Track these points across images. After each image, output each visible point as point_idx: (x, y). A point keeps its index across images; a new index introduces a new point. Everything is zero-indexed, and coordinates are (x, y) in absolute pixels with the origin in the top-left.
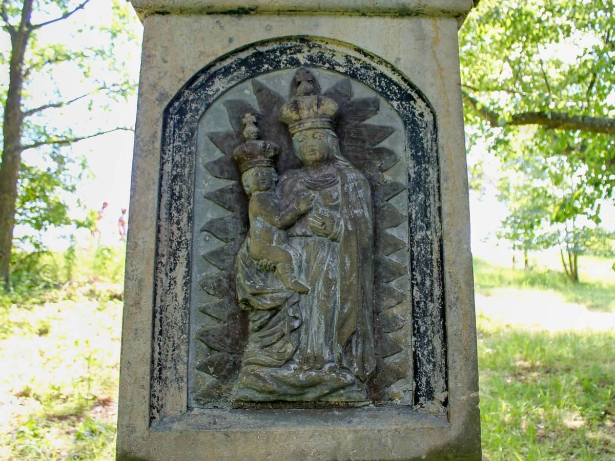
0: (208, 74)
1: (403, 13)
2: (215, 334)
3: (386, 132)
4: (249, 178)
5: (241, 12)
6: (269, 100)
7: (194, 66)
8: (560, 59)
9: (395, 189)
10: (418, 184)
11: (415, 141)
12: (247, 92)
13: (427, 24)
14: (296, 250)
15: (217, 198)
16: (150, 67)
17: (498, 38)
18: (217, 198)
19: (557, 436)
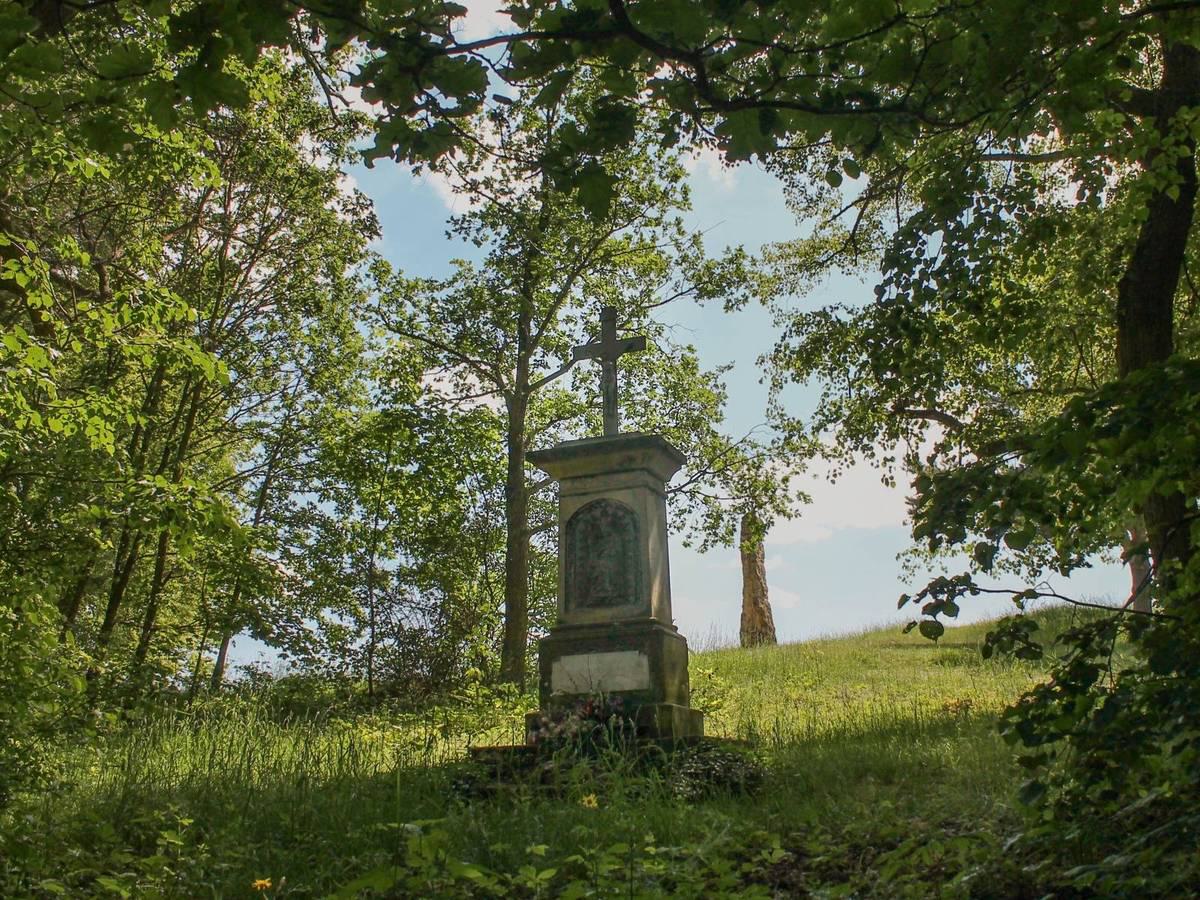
0: (577, 514)
1: (628, 488)
2: (762, 511)
3: (627, 524)
4: (590, 541)
5: (584, 494)
6: (594, 519)
7: (573, 511)
8: (801, 386)
9: (629, 541)
10: (636, 538)
11: (635, 527)
12: (589, 517)
13: (637, 490)
14: (602, 562)
15: (582, 549)
16: (467, 396)
17: (807, 274)
18: (582, 549)
19: (876, 802)
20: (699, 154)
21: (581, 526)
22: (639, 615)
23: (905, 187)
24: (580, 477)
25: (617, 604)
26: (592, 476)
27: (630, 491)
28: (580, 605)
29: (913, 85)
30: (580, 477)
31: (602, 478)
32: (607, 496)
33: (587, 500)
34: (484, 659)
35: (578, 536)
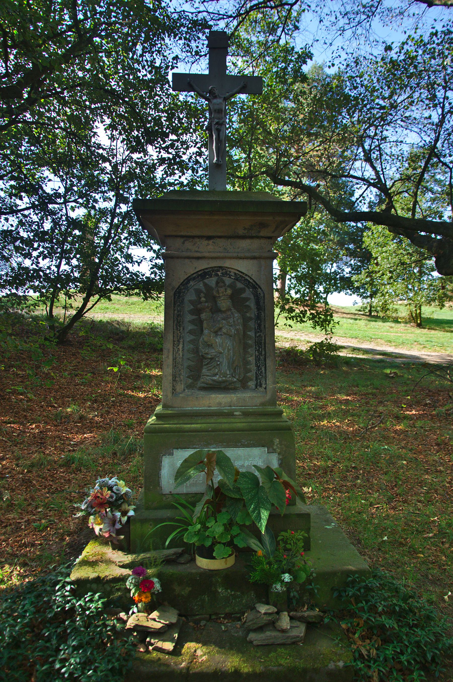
0: (188, 280)
1: (254, 258)
3: (248, 299)
5: (198, 258)
7: (183, 277)
12: (201, 286)
20: (3, 226)
21: (190, 296)
22: (263, 404)
23: (394, 315)
24: (193, 237)
25: (235, 389)
26: (209, 238)
27: (255, 261)
28: (190, 387)
29: (128, 654)
30: (193, 237)
31: (221, 242)
32: (227, 264)
33: (203, 265)
34: (175, 294)
35: (188, 307)
